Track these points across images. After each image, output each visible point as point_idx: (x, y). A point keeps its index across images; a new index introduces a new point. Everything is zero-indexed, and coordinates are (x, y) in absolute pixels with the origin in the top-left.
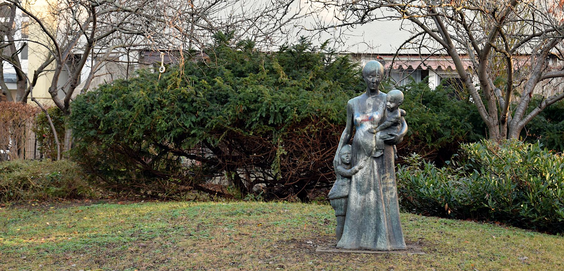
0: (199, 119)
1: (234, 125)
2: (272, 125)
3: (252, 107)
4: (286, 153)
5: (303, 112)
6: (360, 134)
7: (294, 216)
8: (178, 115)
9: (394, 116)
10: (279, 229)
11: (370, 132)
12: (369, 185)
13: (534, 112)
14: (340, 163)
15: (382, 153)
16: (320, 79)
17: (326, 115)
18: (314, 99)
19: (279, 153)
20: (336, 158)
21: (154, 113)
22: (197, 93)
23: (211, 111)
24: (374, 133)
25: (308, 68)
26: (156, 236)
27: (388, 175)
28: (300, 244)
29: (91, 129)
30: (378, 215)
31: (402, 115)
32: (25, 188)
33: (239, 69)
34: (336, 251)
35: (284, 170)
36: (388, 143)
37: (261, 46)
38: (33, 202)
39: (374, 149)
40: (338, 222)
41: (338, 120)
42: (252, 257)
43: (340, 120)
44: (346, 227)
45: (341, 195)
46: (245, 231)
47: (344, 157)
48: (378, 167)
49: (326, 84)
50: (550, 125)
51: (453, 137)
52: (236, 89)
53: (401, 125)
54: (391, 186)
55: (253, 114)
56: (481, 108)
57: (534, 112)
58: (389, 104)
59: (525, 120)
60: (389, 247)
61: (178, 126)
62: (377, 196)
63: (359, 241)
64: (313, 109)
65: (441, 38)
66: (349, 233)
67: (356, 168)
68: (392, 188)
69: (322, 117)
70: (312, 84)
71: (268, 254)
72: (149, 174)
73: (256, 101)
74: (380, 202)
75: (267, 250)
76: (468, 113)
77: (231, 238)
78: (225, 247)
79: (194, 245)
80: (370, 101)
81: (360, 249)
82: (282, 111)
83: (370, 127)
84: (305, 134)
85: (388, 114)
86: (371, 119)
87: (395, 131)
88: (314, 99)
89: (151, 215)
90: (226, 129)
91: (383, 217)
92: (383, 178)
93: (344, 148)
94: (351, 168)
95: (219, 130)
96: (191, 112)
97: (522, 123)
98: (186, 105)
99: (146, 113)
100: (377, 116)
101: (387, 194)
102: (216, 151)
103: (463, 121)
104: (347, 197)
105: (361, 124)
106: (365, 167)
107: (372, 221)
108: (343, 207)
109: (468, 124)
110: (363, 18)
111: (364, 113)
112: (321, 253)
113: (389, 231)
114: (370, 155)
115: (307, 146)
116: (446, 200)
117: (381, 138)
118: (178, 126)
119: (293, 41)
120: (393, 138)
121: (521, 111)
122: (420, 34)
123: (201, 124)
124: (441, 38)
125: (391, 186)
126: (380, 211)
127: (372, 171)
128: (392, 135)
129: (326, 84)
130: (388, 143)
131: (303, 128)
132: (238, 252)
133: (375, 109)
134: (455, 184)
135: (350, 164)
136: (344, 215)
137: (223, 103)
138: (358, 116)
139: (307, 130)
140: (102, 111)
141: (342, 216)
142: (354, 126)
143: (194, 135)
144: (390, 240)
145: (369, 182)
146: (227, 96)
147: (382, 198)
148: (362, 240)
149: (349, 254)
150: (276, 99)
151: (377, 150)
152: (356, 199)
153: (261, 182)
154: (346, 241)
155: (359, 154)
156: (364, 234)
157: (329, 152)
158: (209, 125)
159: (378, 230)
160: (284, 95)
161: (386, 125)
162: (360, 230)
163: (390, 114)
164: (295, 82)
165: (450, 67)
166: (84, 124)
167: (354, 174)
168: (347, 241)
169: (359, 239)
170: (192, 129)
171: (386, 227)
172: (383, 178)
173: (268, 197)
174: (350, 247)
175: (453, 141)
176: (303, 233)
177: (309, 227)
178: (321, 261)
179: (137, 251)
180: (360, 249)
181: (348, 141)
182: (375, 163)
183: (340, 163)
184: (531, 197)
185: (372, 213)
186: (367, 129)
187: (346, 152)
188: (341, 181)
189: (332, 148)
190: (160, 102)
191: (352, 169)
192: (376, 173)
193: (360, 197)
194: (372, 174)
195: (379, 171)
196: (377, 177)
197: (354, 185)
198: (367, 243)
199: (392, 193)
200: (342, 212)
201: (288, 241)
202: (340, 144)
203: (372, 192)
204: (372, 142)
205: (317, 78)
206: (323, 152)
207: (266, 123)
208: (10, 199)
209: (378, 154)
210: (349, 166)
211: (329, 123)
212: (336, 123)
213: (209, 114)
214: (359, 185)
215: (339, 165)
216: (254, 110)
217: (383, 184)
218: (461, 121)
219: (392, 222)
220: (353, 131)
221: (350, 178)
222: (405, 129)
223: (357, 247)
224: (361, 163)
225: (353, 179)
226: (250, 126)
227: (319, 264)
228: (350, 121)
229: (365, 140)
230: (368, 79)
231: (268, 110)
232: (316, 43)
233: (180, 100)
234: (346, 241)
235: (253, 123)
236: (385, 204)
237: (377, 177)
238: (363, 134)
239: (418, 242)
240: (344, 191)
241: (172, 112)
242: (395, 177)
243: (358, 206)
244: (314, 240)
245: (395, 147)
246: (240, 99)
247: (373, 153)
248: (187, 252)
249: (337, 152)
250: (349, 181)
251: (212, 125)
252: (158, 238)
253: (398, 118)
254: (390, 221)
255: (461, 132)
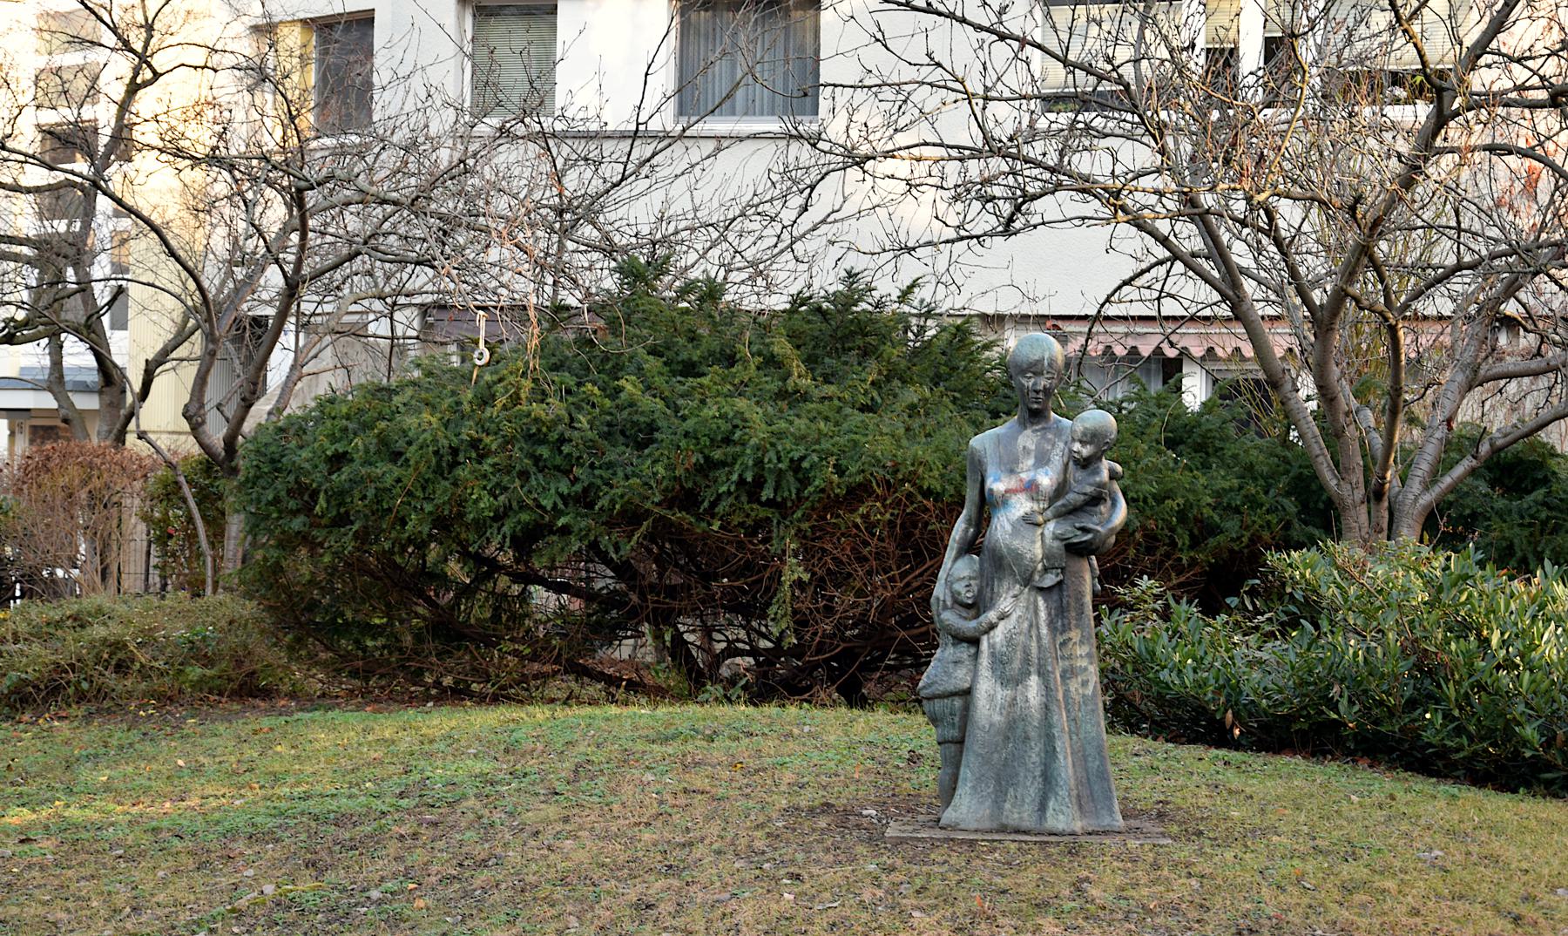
0: (578, 487)
1: (669, 503)
2: (770, 503)
3: (717, 455)
4: (806, 577)
5: (853, 469)
6: (1002, 528)
7: (827, 742)
8: (524, 475)
9: (1091, 480)
10: (788, 777)
11: (1029, 521)
12: (1027, 660)
13: (1459, 470)
14: (949, 603)
15: (1061, 577)
16: (896, 383)
17: (912, 478)
18: (881, 434)
19: (788, 578)
20: (939, 590)
21: (462, 473)
22: (572, 419)
23: (610, 465)
24: (1039, 525)
25: (866, 353)
26: (464, 797)
27: (1075, 635)
28: (845, 817)
29: (295, 513)
30: (1049, 739)
31: (1113, 476)
32: (122, 668)
33: (684, 356)
34: (939, 834)
35: (801, 622)
36: (1076, 550)
37: (742, 295)
38: (140, 707)
39: (1040, 567)
40: (945, 759)
41: (944, 490)
42: (719, 852)
43: (951, 489)
44: (965, 772)
45: (951, 688)
46: (699, 782)
47: (959, 587)
48: (1049, 614)
49: (911, 395)
50: (1500, 504)
51: (1247, 534)
52: (677, 409)
53: (1109, 502)
54: (1084, 663)
55: (721, 474)
56: (1321, 459)
57: (1459, 470)
58: (1077, 446)
59: (1436, 491)
60: (1078, 826)
61: (523, 507)
62: (1048, 689)
63: (1000, 808)
64: (879, 461)
65: (1216, 274)
66: (974, 788)
67: (992, 615)
68: (1086, 669)
69: (903, 481)
70: (875, 394)
71: (759, 844)
72: (449, 632)
73: (727, 441)
74: (1054, 708)
75: (759, 834)
76: (1287, 472)
77: (661, 803)
78: (648, 824)
79: (566, 820)
80: (1028, 439)
81: (1003, 829)
82: (796, 466)
83: (1028, 509)
84: (856, 526)
85: (1075, 474)
86: (1031, 488)
87: (1095, 519)
88: (881, 434)
89: (452, 740)
90: (648, 513)
91: (1063, 745)
92: (1063, 644)
93: (961, 563)
94: (977, 616)
95: (631, 517)
96: (557, 468)
97: (1427, 498)
98: (544, 451)
99: (439, 471)
100: (1046, 480)
101: (1074, 685)
102: (623, 570)
103: (1272, 492)
104: (967, 693)
105: (1004, 501)
106: (1014, 614)
107: (1034, 756)
108: (957, 719)
109: (1285, 502)
110: (1011, 220)
111: (1012, 471)
112: (901, 841)
113: (1079, 783)
114: (1027, 581)
115: (862, 560)
116: (1228, 701)
117: (1056, 538)
118: (523, 507)
119: (827, 282)
120: (1089, 536)
121: (1425, 466)
122: (1161, 263)
123: (585, 499)
124: (1216, 274)
125: (1084, 663)
126: (1055, 731)
127: (1034, 625)
128: (1085, 530)
129: (911, 395)
130: (1076, 550)
131: (853, 511)
132: (680, 839)
133: (1042, 460)
134: (1246, 657)
135: (976, 607)
136: (960, 742)
137: (641, 446)
138: (997, 480)
139: (862, 516)
140: (323, 467)
141: (956, 745)
142: (987, 506)
143: (565, 531)
144: (1080, 807)
145: (1026, 653)
146: (652, 428)
147: (1060, 696)
148: (1007, 806)
149: (972, 843)
150: (780, 435)
151: (1046, 570)
152: (991, 698)
153: (742, 653)
154: (964, 809)
155: (1000, 580)
156: (1011, 790)
157: (921, 575)
158: (603, 502)
159: (1048, 779)
160: (801, 424)
161: (1071, 504)
162: (1002, 781)
163: (1080, 474)
164: (830, 390)
165: (1238, 349)
166: (276, 501)
167: (987, 632)
168: (967, 808)
169: (998, 804)
170: (560, 513)
171: (1070, 771)
172: (1063, 644)
173: (760, 693)
174: (974, 826)
175: (1247, 546)
176: (853, 787)
177: (867, 772)
178: (899, 862)
179: (415, 836)
180: (1003, 829)
181: (971, 547)
182: (1041, 603)
183: (949, 603)
184: (1452, 693)
185: (1033, 734)
186: (1021, 513)
187: (966, 573)
188: (951, 650)
189: (929, 563)
190: (474, 443)
191: (982, 618)
192: (1044, 631)
193: (1002, 694)
194: (1034, 633)
195: (1051, 624)
196: (1046, 641)
197: (985, 660)
198: (1020, 813)
199: (1085, 684)
200: (954, 733)
201: (811, 810)
202: (950, 554)
203: (1034, 681)
204: (1034, 548)
205: (888, 379)
206: (903, 575)
207: (754, 497)
208: (81, 697)
209: (1050, 580)
210: (972, 612)
211: (920, 498)
212: (938, 497)
213: (606, 474)
214: (999, 661)
215: (945, 608)
216: (723, 464)
217: (1063, 658)
218: (1266, 493)
219: (1085, 758)
220: (982, 519)
221: (975, 642)
222: (1121, 514)
223: (995, 826)
224: (1005, 603)
225: (984, 645)
226: (714, 504)
227: (893, 869)
228: (977, 492)
229: (1016, 543)
230: (1024, 381)
231: (759, 463)
232: (887, 288)
233: (529, 437)
234: (964, 809)
235: (719, 497)
236: (1068, 711)
237: (1046, 641)
238: (1008, 528)
239: (1154, 813)
240: (961, 678)
241: (508, 470)
242: (1094, 640)
243: (997, 718)
244: (881, 805)
245: (1095, 562)
246: (686, 435)
247: (1037, 577)
248: (547, 837)
249: (942, 574)
250: (973, 650)
251: (613, 502)
252: (472, 802)
253: (1101, 485)
254: (1081, 757)
255: (1268, 523)
